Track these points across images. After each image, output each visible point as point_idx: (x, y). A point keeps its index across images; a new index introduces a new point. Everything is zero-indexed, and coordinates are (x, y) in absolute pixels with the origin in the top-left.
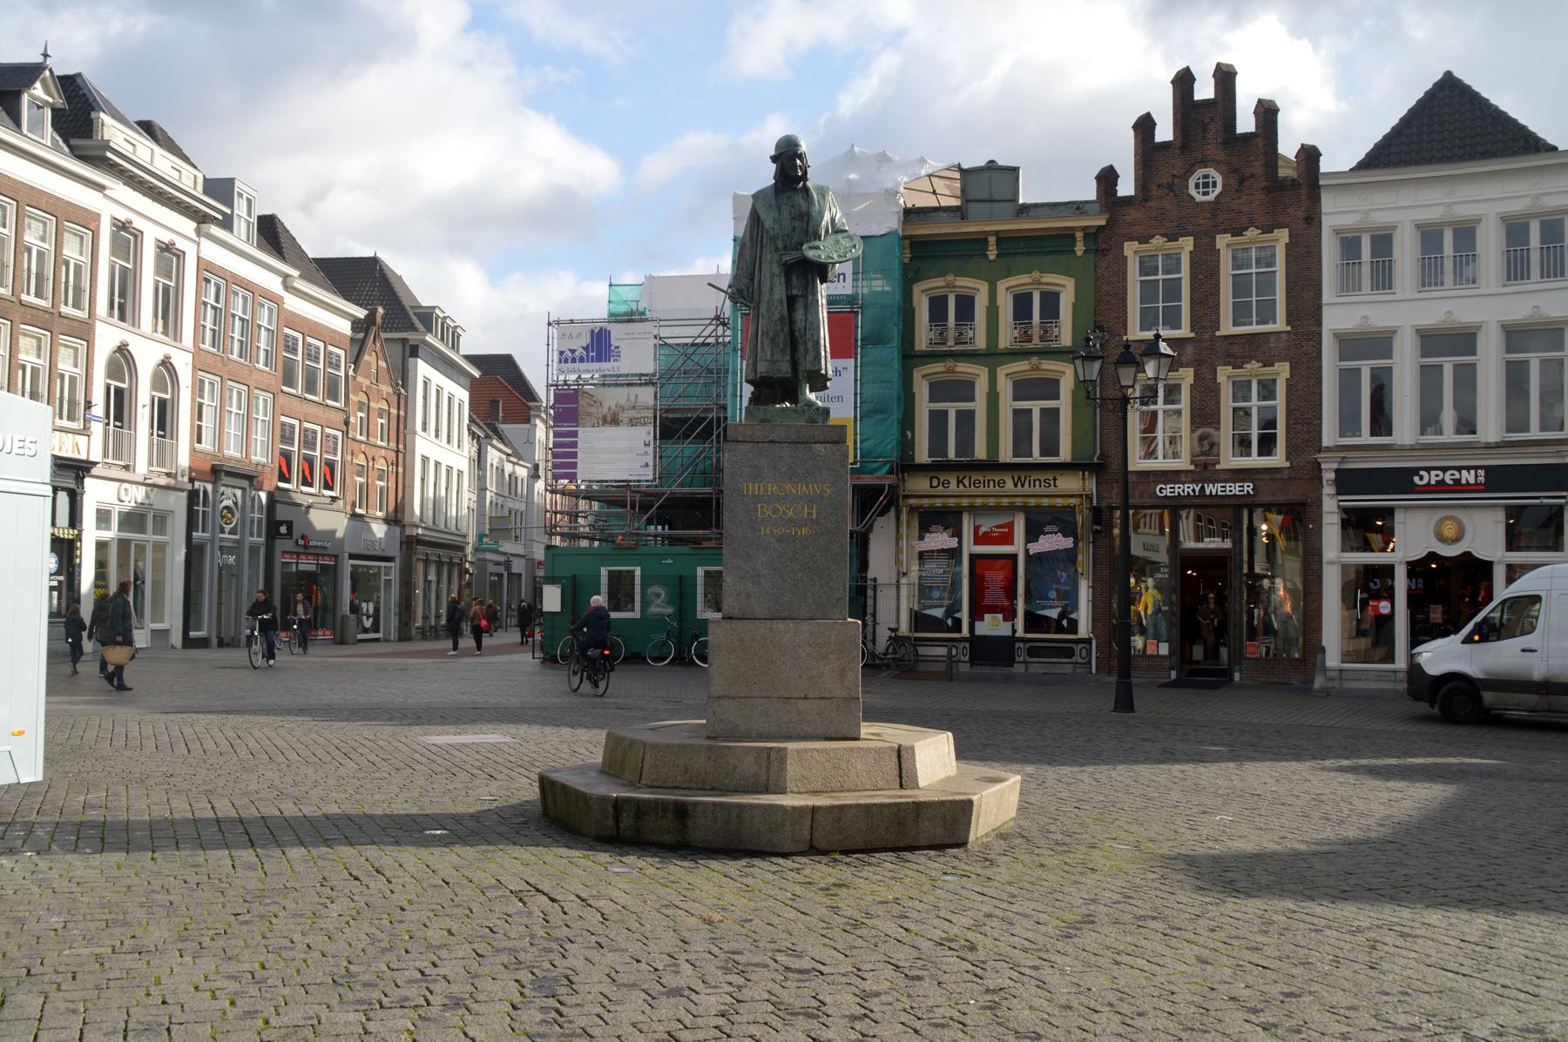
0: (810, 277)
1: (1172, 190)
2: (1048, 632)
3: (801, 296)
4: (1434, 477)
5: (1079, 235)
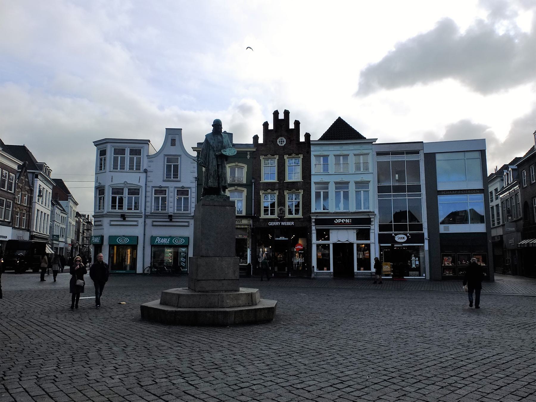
1: (273, 142)
2: (329, 254)
4: (339, 221)
5: (248, 153)
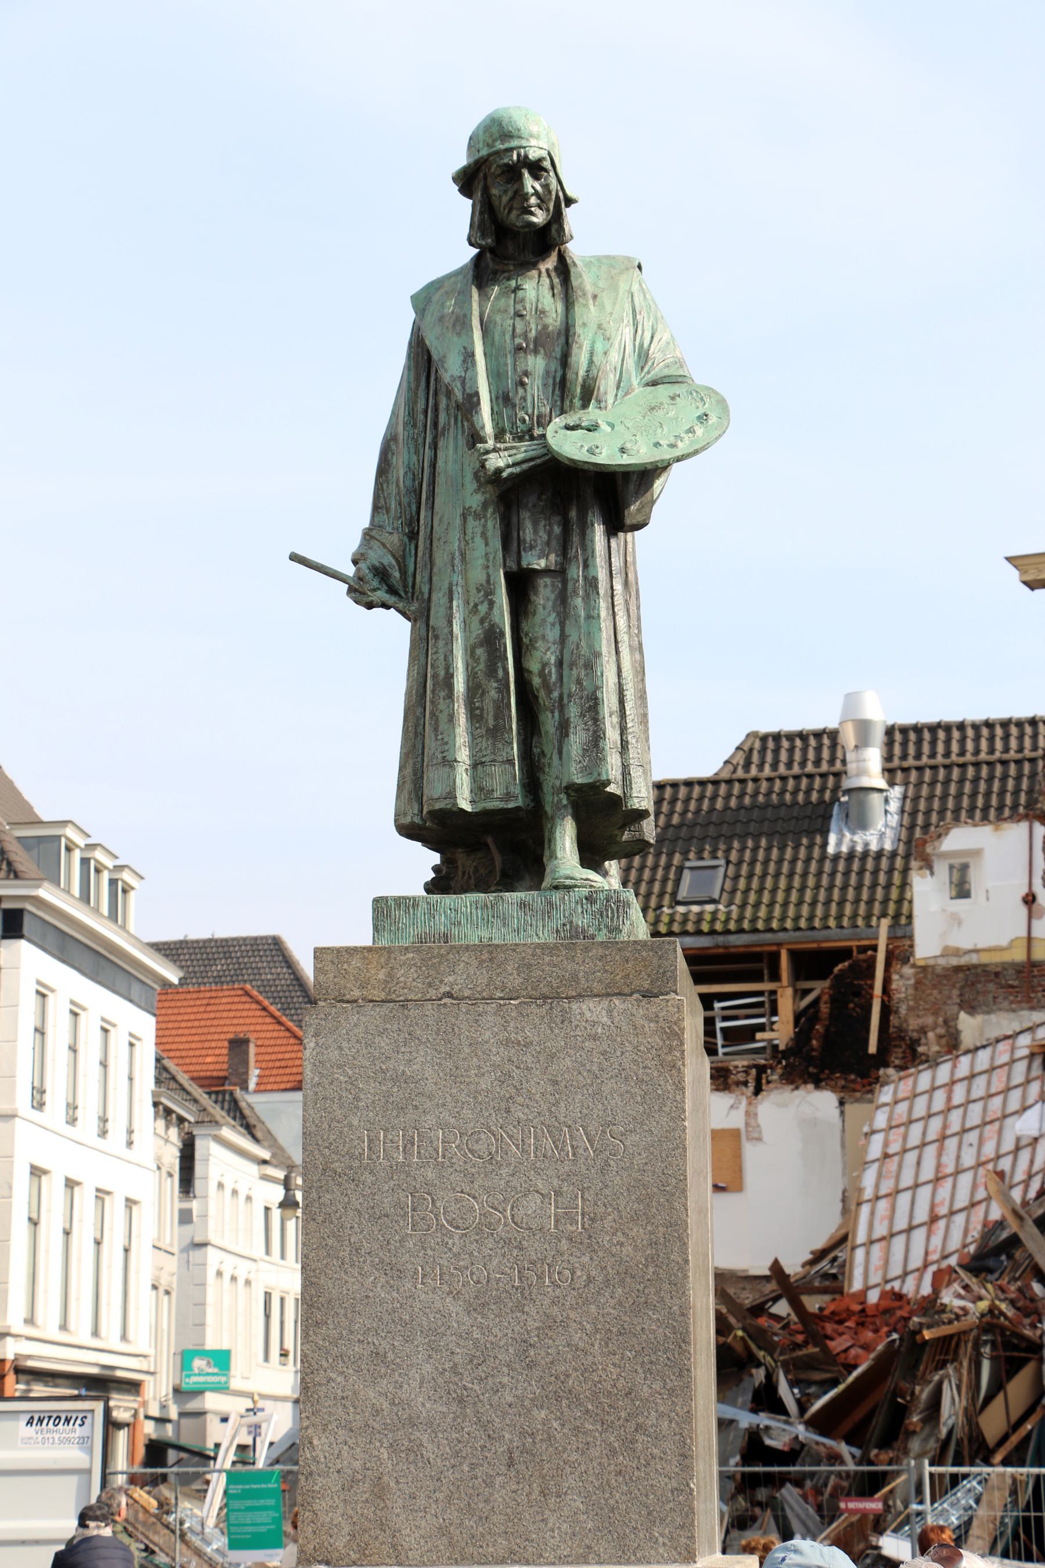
0: (573, 514)
3: (546, 572)
